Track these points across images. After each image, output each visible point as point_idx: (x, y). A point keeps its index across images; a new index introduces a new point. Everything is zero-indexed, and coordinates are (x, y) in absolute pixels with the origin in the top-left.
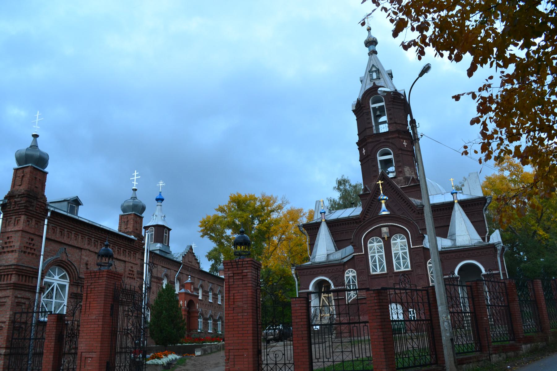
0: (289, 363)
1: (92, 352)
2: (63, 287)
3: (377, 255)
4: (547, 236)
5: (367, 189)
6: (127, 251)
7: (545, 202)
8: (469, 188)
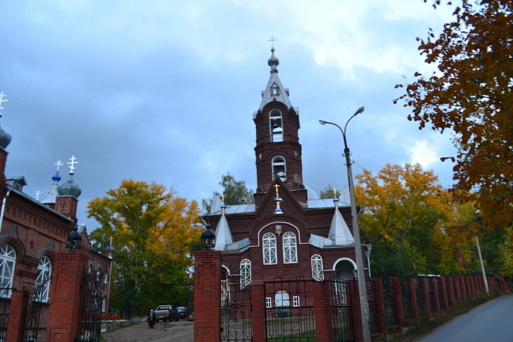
0: (248, 339)
1: (62, 328)
2: (10, 264)
3: (270, 249)
4: (391, 240)
5: (260, 189)
6: (63, 232)
7: (392, 212)
8: (345, 197)
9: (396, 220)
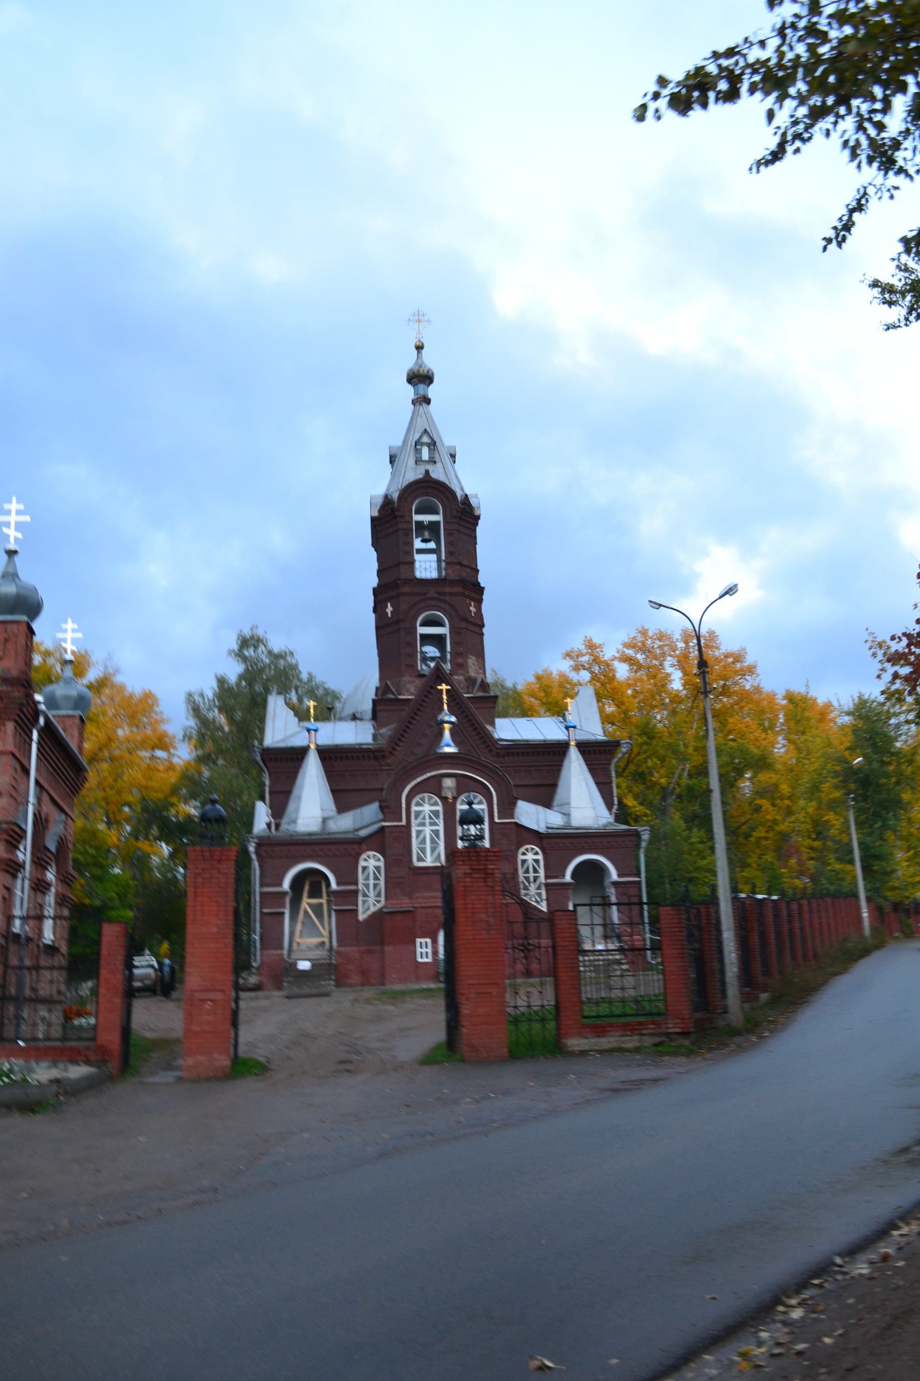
3: (428, 830)
4: (639, 811)
7: (646, 744)
8: (579, 715)
9: (655, 764)
